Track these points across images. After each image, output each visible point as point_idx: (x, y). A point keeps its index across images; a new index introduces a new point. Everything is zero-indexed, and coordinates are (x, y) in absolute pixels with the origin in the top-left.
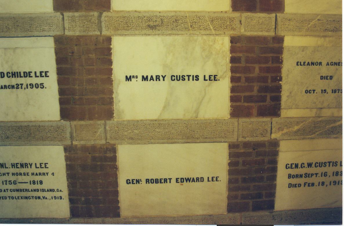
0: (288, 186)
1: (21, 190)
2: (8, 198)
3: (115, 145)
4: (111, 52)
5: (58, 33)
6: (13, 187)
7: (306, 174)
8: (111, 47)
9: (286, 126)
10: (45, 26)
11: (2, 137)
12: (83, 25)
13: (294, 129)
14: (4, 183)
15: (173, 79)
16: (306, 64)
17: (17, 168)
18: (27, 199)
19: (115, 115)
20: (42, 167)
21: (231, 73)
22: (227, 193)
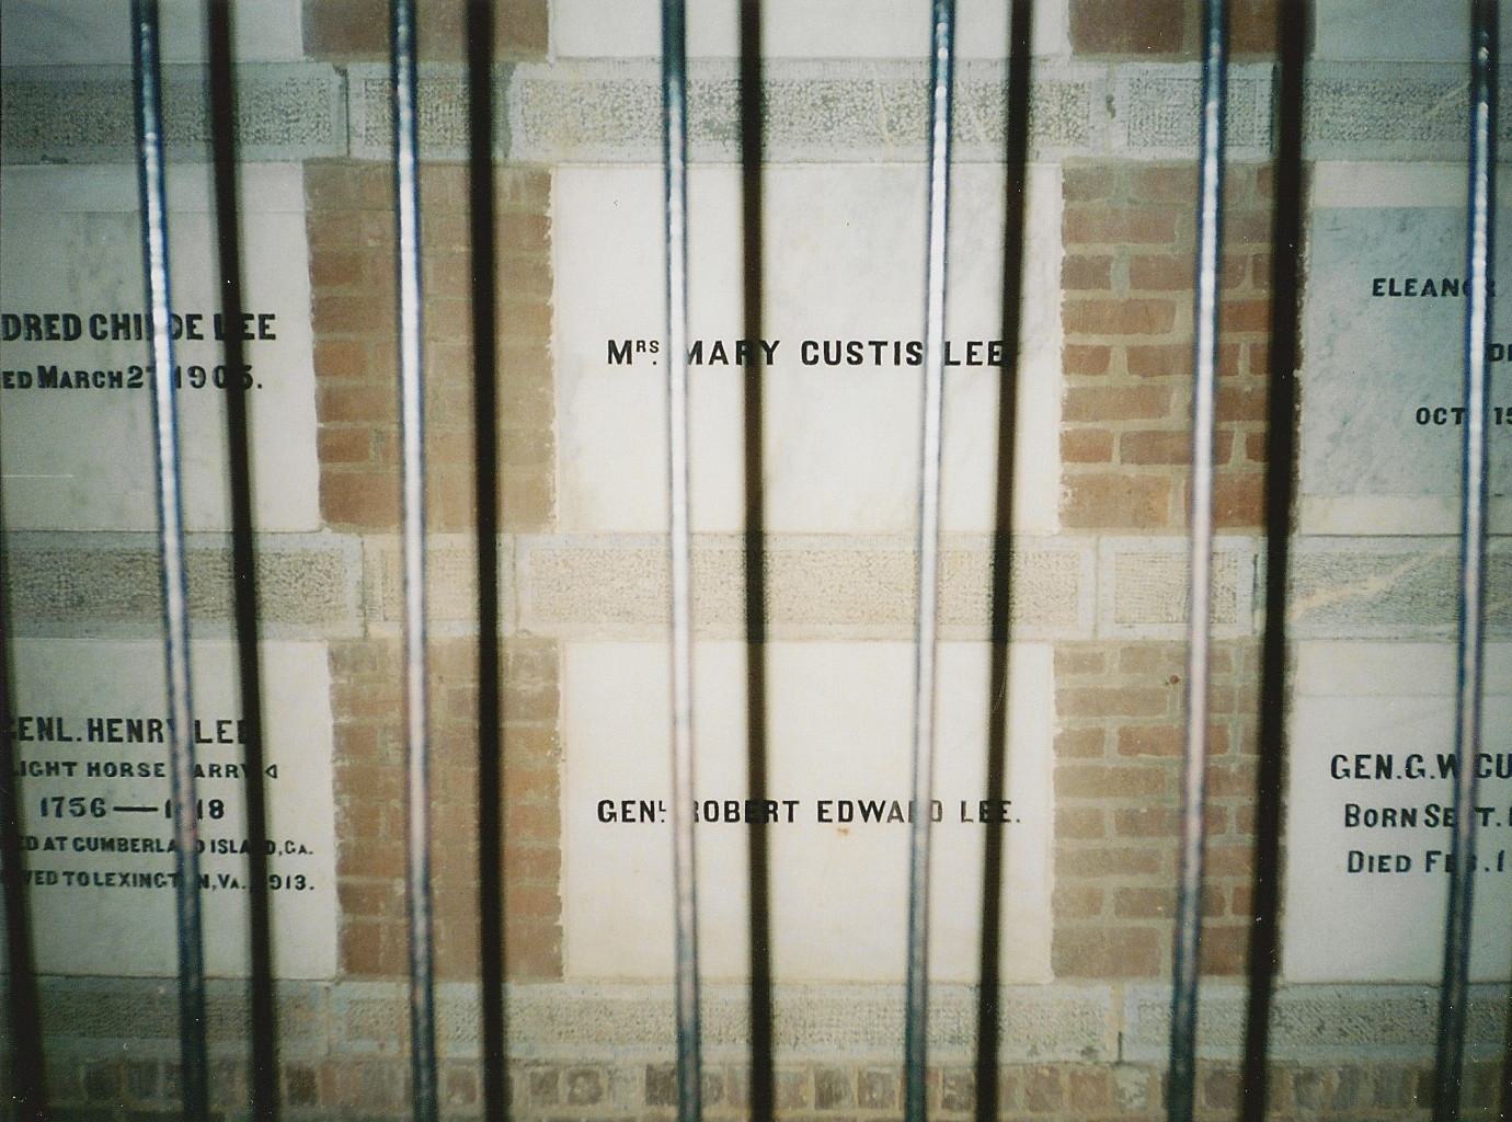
0: (1346, 864)
1: (124, 845)
2: (63, 879)
3: (552, 642)
4: (549, 237)
5: (321, 152)
6: (88, 827)
7: (1433, 810)
8: (548, 215)
9: (1327, 574)
10: (266, 118)
11: (53, 601)
12: (431, 120)
13: (1365, 589)
14: (52, 806)
15: (810, 358)
16: (1418, 287)
17: (112, 739)
18: (149, 885)
19: (557, 508)
20: (224, 737)
21: (1066, 333)
22: (1052, 879)
